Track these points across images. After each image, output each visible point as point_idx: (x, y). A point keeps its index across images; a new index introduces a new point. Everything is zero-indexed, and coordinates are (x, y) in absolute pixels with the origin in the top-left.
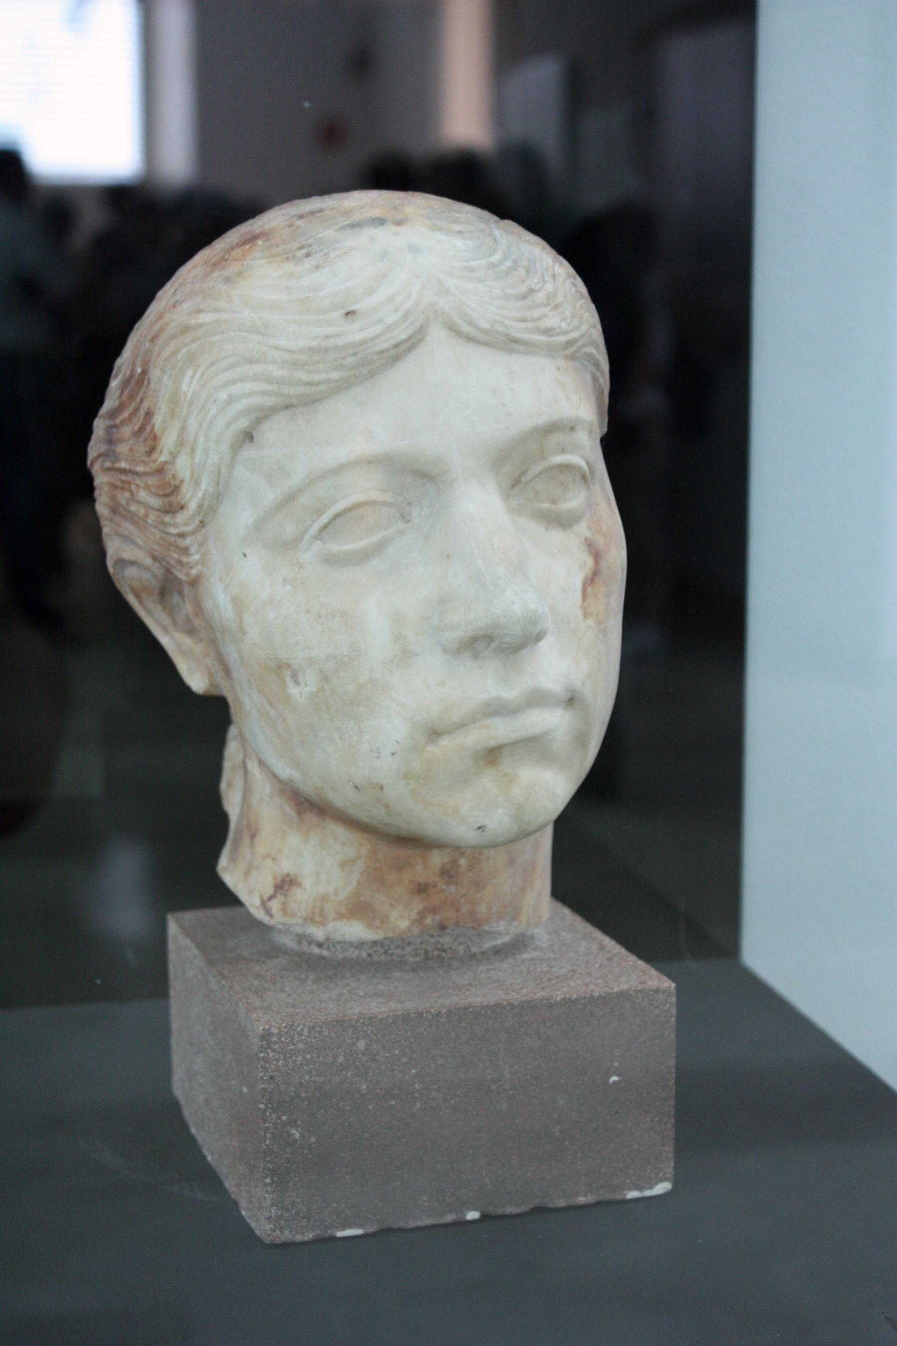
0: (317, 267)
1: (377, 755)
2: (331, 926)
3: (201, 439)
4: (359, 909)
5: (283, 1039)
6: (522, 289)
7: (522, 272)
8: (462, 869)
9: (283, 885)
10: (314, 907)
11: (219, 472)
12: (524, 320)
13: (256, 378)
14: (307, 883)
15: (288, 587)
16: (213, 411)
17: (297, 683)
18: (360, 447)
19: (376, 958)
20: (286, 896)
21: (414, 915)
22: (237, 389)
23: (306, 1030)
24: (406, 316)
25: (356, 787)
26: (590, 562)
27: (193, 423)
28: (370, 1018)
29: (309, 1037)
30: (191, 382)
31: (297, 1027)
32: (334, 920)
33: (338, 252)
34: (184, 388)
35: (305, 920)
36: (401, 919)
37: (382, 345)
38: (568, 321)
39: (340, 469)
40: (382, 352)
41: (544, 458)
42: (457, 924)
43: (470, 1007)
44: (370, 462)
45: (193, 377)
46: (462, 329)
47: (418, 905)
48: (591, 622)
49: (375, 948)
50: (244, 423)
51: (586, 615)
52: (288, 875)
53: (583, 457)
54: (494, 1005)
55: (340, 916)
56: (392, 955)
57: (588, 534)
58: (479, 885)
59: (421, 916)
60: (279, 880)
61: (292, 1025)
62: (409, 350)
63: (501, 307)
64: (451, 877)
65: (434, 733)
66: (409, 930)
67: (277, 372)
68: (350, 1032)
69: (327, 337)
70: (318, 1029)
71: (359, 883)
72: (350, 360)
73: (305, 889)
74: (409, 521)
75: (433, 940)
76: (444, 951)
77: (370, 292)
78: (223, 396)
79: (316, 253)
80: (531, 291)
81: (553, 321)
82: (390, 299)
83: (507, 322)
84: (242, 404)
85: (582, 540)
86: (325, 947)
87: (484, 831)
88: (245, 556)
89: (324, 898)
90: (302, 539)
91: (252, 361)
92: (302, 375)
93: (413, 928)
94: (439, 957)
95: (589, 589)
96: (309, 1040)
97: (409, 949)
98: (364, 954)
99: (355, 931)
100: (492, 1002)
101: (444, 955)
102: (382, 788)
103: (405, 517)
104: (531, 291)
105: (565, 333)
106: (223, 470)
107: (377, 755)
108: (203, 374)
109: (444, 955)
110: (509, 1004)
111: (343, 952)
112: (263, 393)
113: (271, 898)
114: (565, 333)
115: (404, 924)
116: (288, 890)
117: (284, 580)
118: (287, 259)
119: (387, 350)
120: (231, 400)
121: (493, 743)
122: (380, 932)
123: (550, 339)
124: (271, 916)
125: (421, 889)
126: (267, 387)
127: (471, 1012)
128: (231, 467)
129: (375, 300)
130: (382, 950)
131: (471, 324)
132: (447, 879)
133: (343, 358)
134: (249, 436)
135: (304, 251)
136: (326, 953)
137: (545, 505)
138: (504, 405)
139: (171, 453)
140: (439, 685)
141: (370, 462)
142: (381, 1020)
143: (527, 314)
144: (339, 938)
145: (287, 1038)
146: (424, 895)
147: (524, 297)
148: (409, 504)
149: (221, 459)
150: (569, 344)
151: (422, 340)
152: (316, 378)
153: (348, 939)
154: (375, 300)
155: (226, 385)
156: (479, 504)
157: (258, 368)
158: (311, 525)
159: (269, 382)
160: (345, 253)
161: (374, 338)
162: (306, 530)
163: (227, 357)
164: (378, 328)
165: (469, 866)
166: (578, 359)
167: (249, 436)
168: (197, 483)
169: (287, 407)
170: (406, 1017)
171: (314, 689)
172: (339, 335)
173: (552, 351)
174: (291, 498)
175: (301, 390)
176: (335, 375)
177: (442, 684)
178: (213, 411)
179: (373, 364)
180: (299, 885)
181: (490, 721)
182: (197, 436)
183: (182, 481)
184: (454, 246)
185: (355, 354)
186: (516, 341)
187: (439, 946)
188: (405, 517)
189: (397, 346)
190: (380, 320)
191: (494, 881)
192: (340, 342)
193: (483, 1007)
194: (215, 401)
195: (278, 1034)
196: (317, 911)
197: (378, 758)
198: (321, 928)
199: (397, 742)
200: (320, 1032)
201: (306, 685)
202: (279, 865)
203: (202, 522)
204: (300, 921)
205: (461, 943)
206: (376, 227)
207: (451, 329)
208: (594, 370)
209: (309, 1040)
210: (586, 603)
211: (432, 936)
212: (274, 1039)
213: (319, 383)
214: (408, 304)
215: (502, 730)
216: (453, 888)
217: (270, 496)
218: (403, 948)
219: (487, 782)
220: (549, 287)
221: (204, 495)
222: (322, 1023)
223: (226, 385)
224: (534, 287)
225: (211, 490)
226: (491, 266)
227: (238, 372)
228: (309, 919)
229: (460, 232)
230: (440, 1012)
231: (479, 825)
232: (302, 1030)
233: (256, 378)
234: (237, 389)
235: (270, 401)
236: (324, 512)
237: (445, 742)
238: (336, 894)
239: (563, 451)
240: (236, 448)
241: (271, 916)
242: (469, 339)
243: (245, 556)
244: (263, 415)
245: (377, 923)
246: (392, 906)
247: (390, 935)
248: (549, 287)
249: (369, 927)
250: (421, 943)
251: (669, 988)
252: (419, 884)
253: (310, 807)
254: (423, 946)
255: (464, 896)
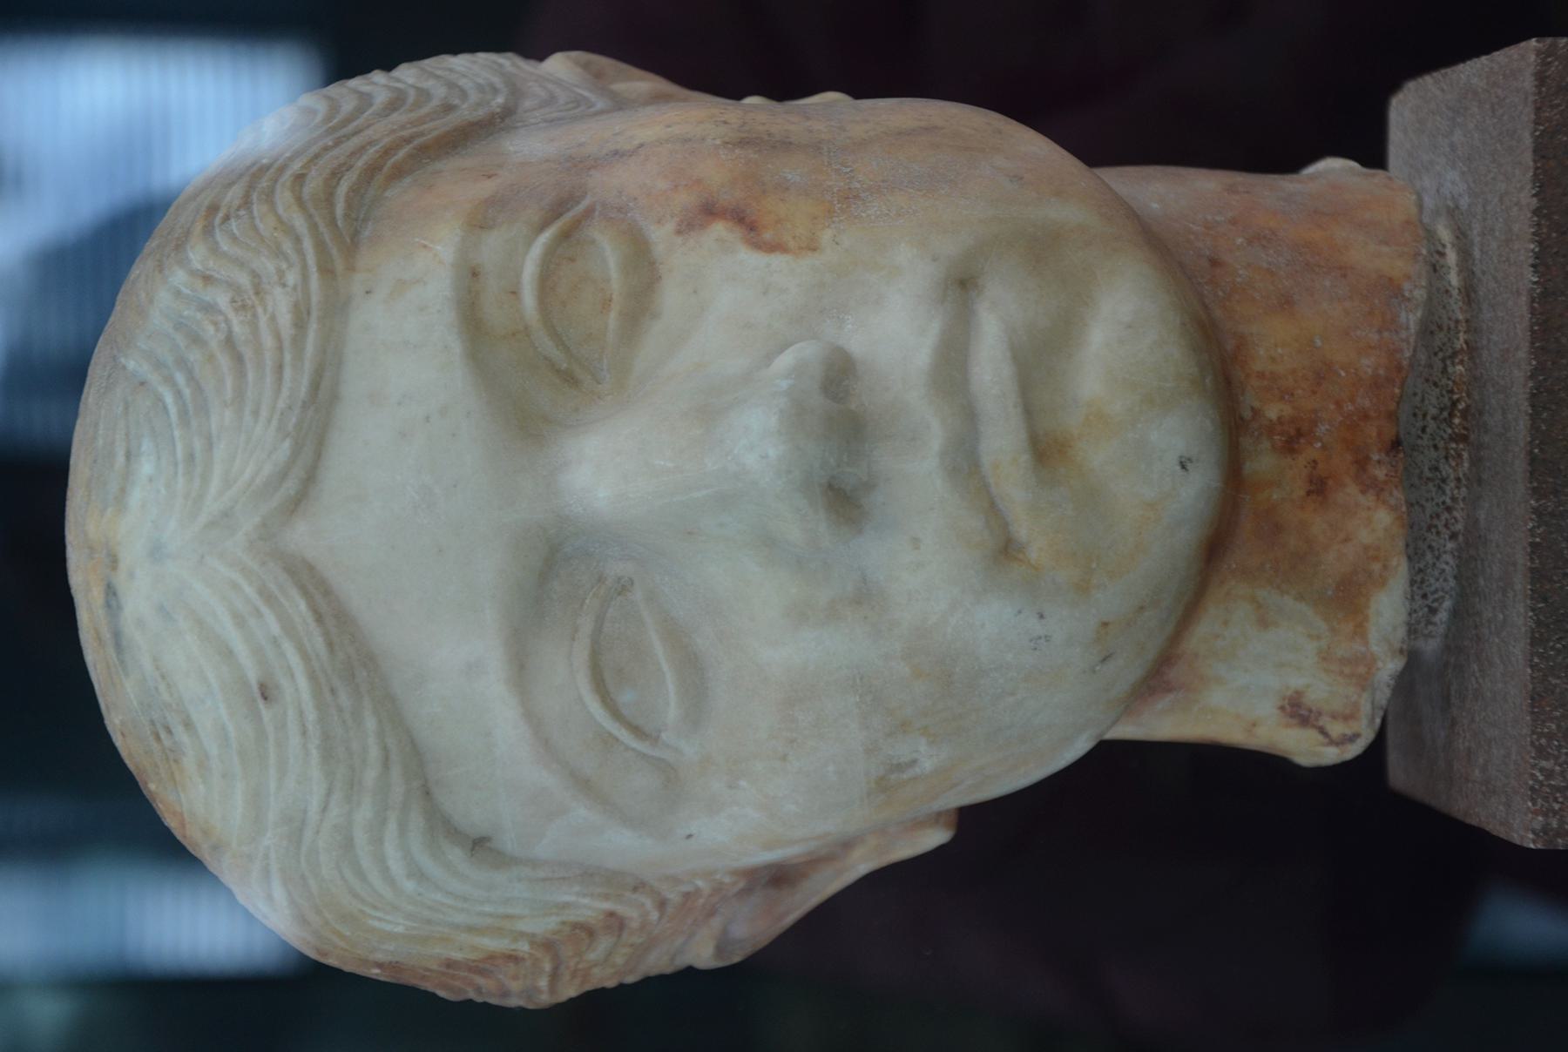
0: (188, 724)
3: (488, 908)
4: (1347, 599)
5: (1556, 806)
6: (224, 361)
7: (195, 356)
10: (1341, 673)
11: (544, 880)
12: (279, 368)
13: (377, 841)
14: (1296, 682)
15: (743, 783)
16: (439, 897)
17: (914, 762)
18: (494, 687)
19: (1459, 527)
20: (1320, 714)
21: (1368, 500)
22: (396, 866)
23: (1544, 763)
24: (269, 598)
25: (1104, 660)
26: (719, 229)
27: (459, 918)
29: (1556, 758)
31: (1536, 780)
32: (1366, 644)
33: (162, 687)
34: (400, 929)
36: (1373, 523)
38: (284, 266)
39: (531, 717)
40: (330, 645)
42: (1392, 416)
43: (1531, 452)
46: (292, 492)
47: (1350, 492)
48: (826, 236)
50: (456, 854)
51: (812, 247)
52: (1282, 708)
53: (529, 243)
54: (1533, 406)
55: (1360, 631)
57: (670, 226)
58: (1322, 374)
61: (1532, 789)
62: (328, 592)
64: (1299, 433)
65: (1006, 550)
66: (1394, 509)
67: (365, 812)
69: (304, 733)
70: (1543, 741)
71: (1300, 597)
72: (344, 699)
73: (1308, 686)
75: (1432, 426)
76: (1454, 404)
77: (228, 654)
78: (409, 886)
80: (229, 342)
81: (281, 303)
82: (239, 621)
83: (281, 404)
85: (679, 240)
86: (1435, 605)
88: (690, 836)
89: (1325, 657)
91: (348, 845)
92: (371, 775)
93: (1393, 502)
94: (1465, 414)
95: (767, 236)
97: (1446, 470)
98: (1450, 545)
99: (1388, 609)
101: (1461, 406)
102: (1105, 624)
103: (624, 587)
104: (229, 342)
106: (541, 874)
108: (375, 908)
109: (1461, 406)
110: (1532, 377)
111: (1445, 580)
112: (403, 829)
113: (1322, 731)
114: (305, 277)
117: (730, 787)
118: (176, 761)
120: (419, 875)
121: (1025, 458)
125: (1319, 488)
126: (392, 827)
127: (1541, 450)
128: (534, 863)
130: (1445, 515)
131: (283, 475)
133: (340, 710)
134: (479, 845)
135: (163, 735)
136: (1447, 604)
137: (613, 319)
138: (427, 419)
139: (515, 940)
142: (1539, 623)
144: (1401, 632)
146: (1330, 482)
147: (239, 359)
148: (601, 579)
149: (520, 880)
150: (327, 271)
151: (311, 568)
152: (374, 752)
156: (604, 468)
157: (361, 838)
159: (384, 822)
160: (163, 677)
161: (305, 656)
164: (288, 647)
165: (1282, 398)
166: (356, 234)
173: (337, 308)
174: (583, 785)
175: (396, 773)
176: (370, 723)
177: (916, 542)
178: (439, 897)
179: (353, 664)
180: (1299, 693)
181: (986, 461)
183: (564, 923)
186: (315, 386)
187: (1445, 414)
188: (624, 587)
189: (319, 619)
190: (275, 642)
191: (1319, 343)
193: (1534, 428)
195: (1545, 815)
196: (1347, 670)
198: (1380, 664)
202: (1281, 686)
203: (635, 889)
208: (380, 178)
210: (792, 244)
211: (1424, 430)
214: (250, 591)
215: (1002, 441)
216: (1322, 429)
217: (582, 812)
218: (1444, 481)
220: (222, 299)
221: (585, 895)
222: (1533, 733)
224: (221, 336)
226: (183, 414)
227: (366, 863)
229: (128, 456)
230: (1535, 511)
231: (1178, 468)
233: (377, 841)
234: (396, 866)
235: (417, 820)
236: (610, 734)
237: (1022, 529)
238: (1318, 637)
239: (515, 293)
242: (311, 478)
243: (690, 836)
244: (442, 827)
245: (1376, 567)
246: (1347, 540)
247: (1401, 544)
248: (222, 299)
249: (1382, 583)
251: (1538, 53)
252: (1309, 493)
253: (1160, 677)
254: (1441, 444)
255: (1338, 404)
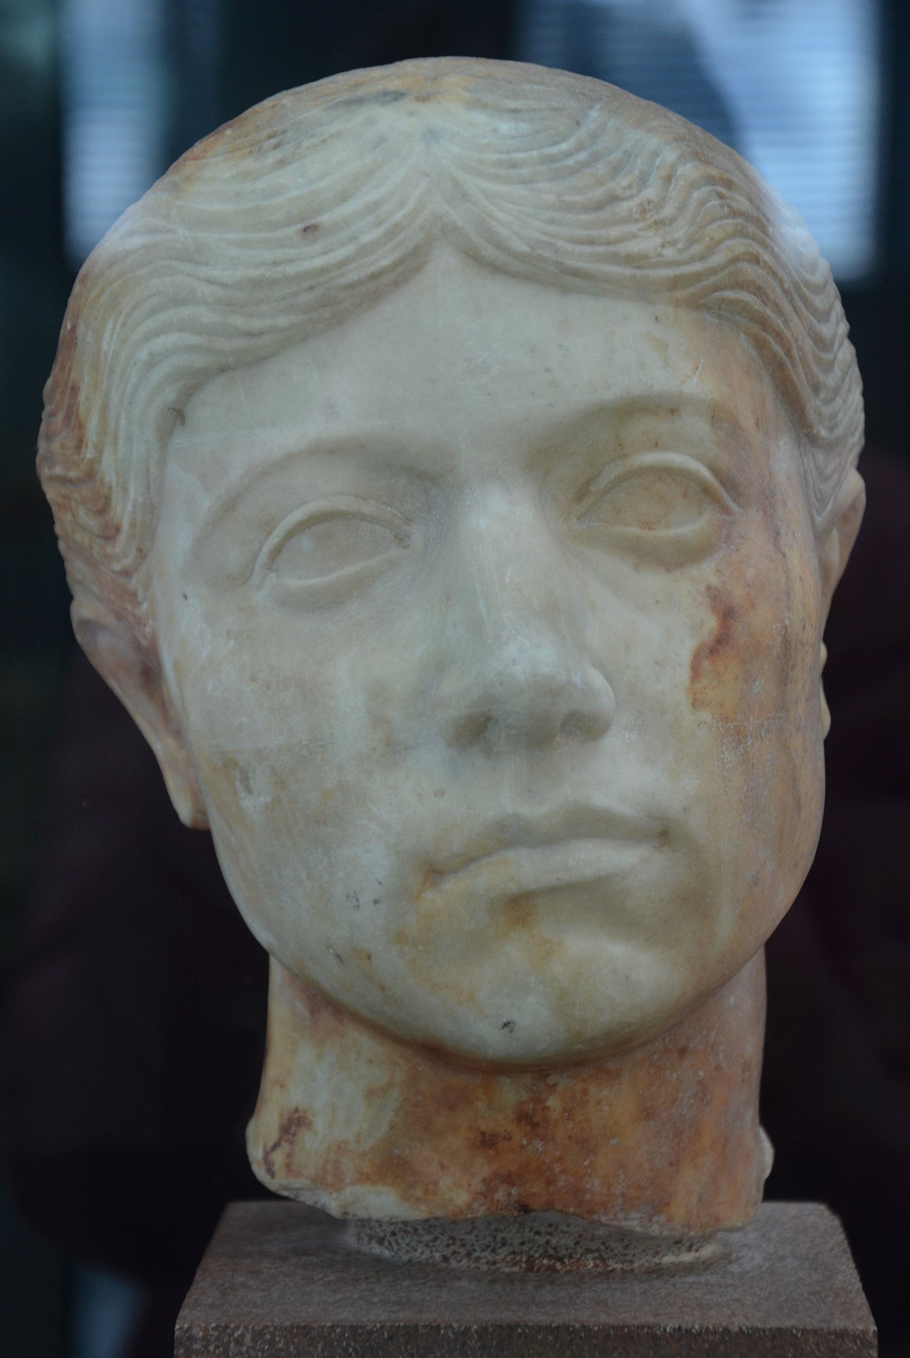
0: (282, 163)
1: (355, 903)
2: (348, 1192)
3: (123, 422)
4: (392, 1167)
5: (211, 1348)
6: (597, 194)
7: (601, 169)
8: (555, 1115)
9: (290, 1127)
10: (327, 1162)
11: (148, 471)
12: (591, 242)
13: (182, 327)
14: (319, 1123)
15: (232, 643)
17: (249, 791)
20: (292, 1143)
22: (159, 343)
23: (248, 1337)
26: (712, 623)
27: (114, 398)
28: (352, 1327)
29: (253, 1348)
30: (111, 336)
32: (352, 1183)
33: (315, 140)
35: (313, 1181)
36: (457, 1189)
37: (353, 275)
38: (680, 246)
39: (289, 460)
40: (351, 286)
41: (626, 456)
44: (332, 452)
45: (115, 324)
47: (483, 1169)
48: (706, 716)
49: (452, 1248)
50: (170, 395)
51: (696, 703)
52: (296, 1110)
54: (558, 1328)
55: (363, 1178)
56: (478, 1259)
57: (714, 580)
58: (586, 1145)
59: (489, 1186)
60: (285, 1121)
61: (227, 1327)
62: (397, 284)
63: (552, 222)
64: (535, 1125)
65: (434, 872)
66: (469, 1207)
67: (206, 316)
68: (320, 1346)
69: (275, 263)
71: (393, 1126)
72: (305, 298)
73: (316, 1133)
74: (406, 547)
75: (541, 1240)
76: (560, 1260)
77: (343, 197)
78: (143, 355)
79: (288, 143)
80: (614, 199)
81: (647, 243)
82: (372, 207)
83: (560, 243)
84: (164, 368)
85: (702, 588)
87: (512, 1030)
88: (185, 597)
89: (341, 1147)
90: (252, 571)
91: (178, 301)
92: (239, 321)
93: (475, 1206)
94: (552, 1268)
96: (253, 1354)
98: (437, 1256)
99: (383, 1202)
100: (558, 1321)
101: (558, 1266)
102: (369, 957)
103: (401, 540)
105: (670, 264)
107: (355, 903)
108: (123, 325)
109: (558, 1266)
111: (407, 1252)
112: (192, 349)
113: (276, 1145)
114: (670, 264)
115: (462, 1198)
116: (294, 1135)
117: (228, 633)
119: (360, 283)
120: (153, 362)
121: (513, 888)
122: (423, 1208)
123: (639, 273)
124: (272, 1174)
125: (487, 1142)
126: (194, 340)
127: (520, 1335)
128: (162, 463)
129: (348, 209)
130: (463, 1251)
131: (499, 245)
132: (528, 1128)
133: (295, 295)
135: (273, 141)
136: (387, 1254)
137: (633, 530)
140: (435, 795)
141: (332, 452)
142: (370, 1332)
143: (601, 233)
144: (362, 1214)
145: (217, 1347)
146: (492, 1152)
147: (599, 206)
150: (675, 283)
152: (258, 324)
153: (375, 1215)
154: (348, 209)
155: (147, 338)
156: (503, 523)
157: (184, 312)
158: (261, 548)
159: (198, 332)
160: (324, 141)
162: (255, 558)
163: (150, 297)
165: (565, 1110)
166: (707, 308)
167: (177, 415)
168: (125, 490)
169: (223, 370)
170: (411, 1331)
171: (268, 799)
172: (292, 261)
173: (643, 292)
175: (240, 343)
176: (283, 321)
178: (133, 380)
179: (334, 306)
180: (309, 1125)
182: (118, 417)
183: (110, 488)
184: (495, 131)
185: (311, 288)
186: (576, 273)
187: (551, 1252)
188: (401, 540)
189: (375, 276)
190: (354, 238)
191: (613, 1142)
192: (290, 269)
193: (539, 1329)
194: (135, 364)
195: (204, 1338)
196: (329, 1167)
197: (357, 907)
198: (334, 1195)
199: (380, 883)
200: (272, 1343)
201: (259, 794)
203: (140, 550)
204: (307, 1182)
205: (589, 1251)
206: (384, 104)
207: (467, 253)
208: (756, 329)
209: (253, 1354)
210: (698, 686)
212: (196, 1346)
213: (261, 334)
215: (527, 868)
216: (538, 1145)
217: (206, 504)
218: (494, 1251)
219: (515, 952)
221: (134, 506)
222: (275, 1328)
223: (147, 338)
224: (619, 192)
225: (140, 500)
227: (163, 317)
228: (319, 1181)
229: (515, 111)
230: (468, 1330)
231: (505, 1020)
232: (243, 1335)
233: (182, 327)
234: (159, 343)
235: (200, 361)
237: (452, 886)
238: (358, 1142)
239: (657, 446)
240: (165, 434)
241: (272, 1174)
242: (496, 269)
243: (185, 597)
244: (194, 383)
245: (419, 1192)
246: (442, 1167)
247: (439, 1213)
248: (651, 192)
250: (523, 1243)
252: (483, 1133)
254: (525, 1248)
255: (560, 1159)
